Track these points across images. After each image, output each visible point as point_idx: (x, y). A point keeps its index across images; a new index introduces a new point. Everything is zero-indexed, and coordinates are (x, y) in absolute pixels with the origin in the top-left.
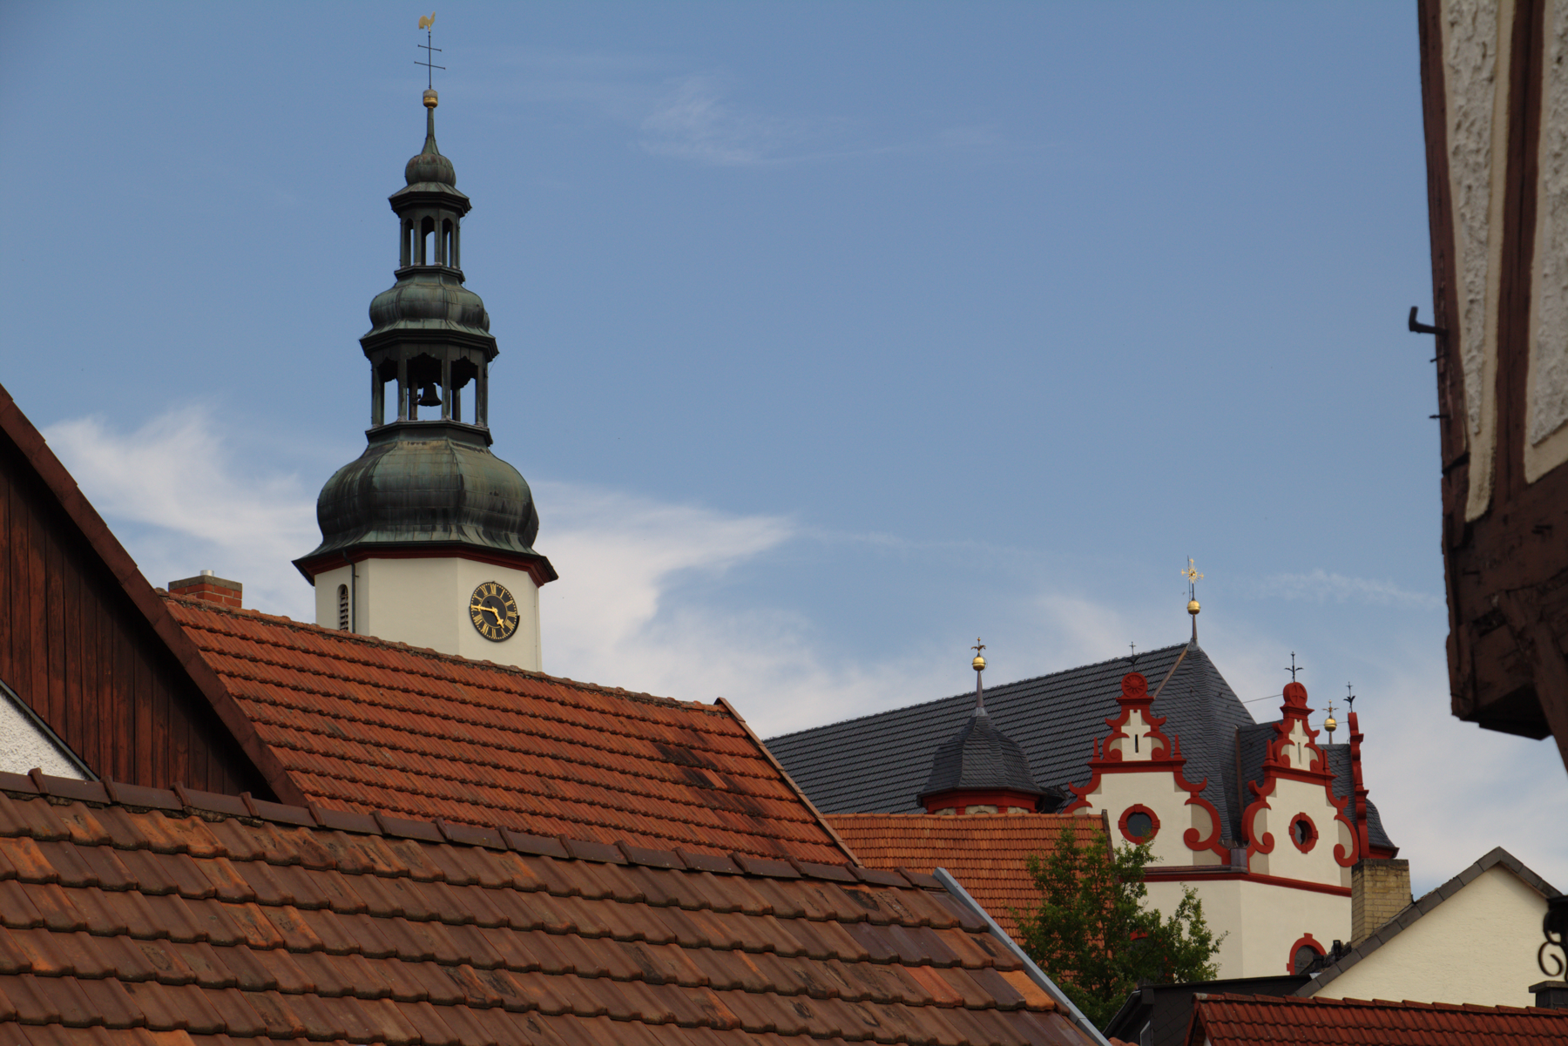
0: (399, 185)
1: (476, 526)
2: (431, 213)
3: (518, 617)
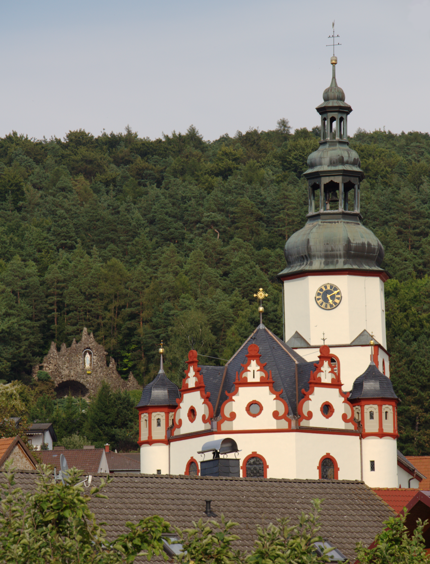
0: (320, 102)
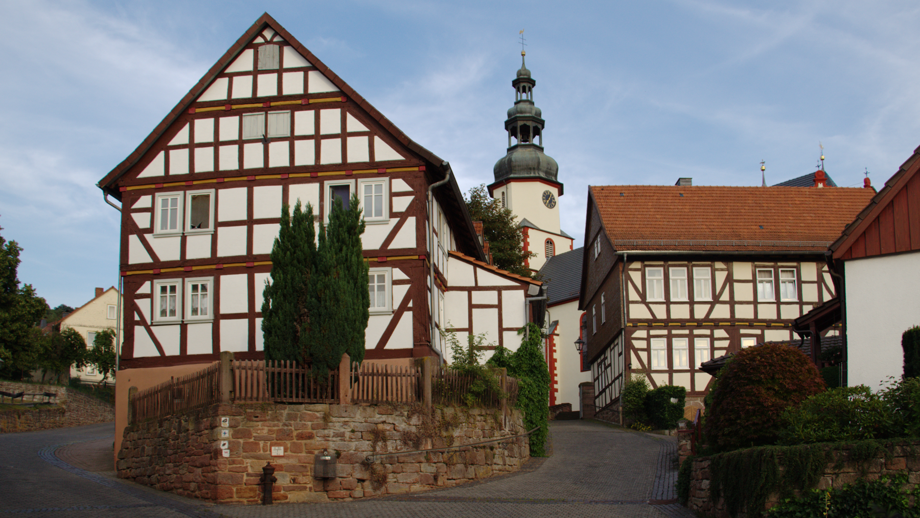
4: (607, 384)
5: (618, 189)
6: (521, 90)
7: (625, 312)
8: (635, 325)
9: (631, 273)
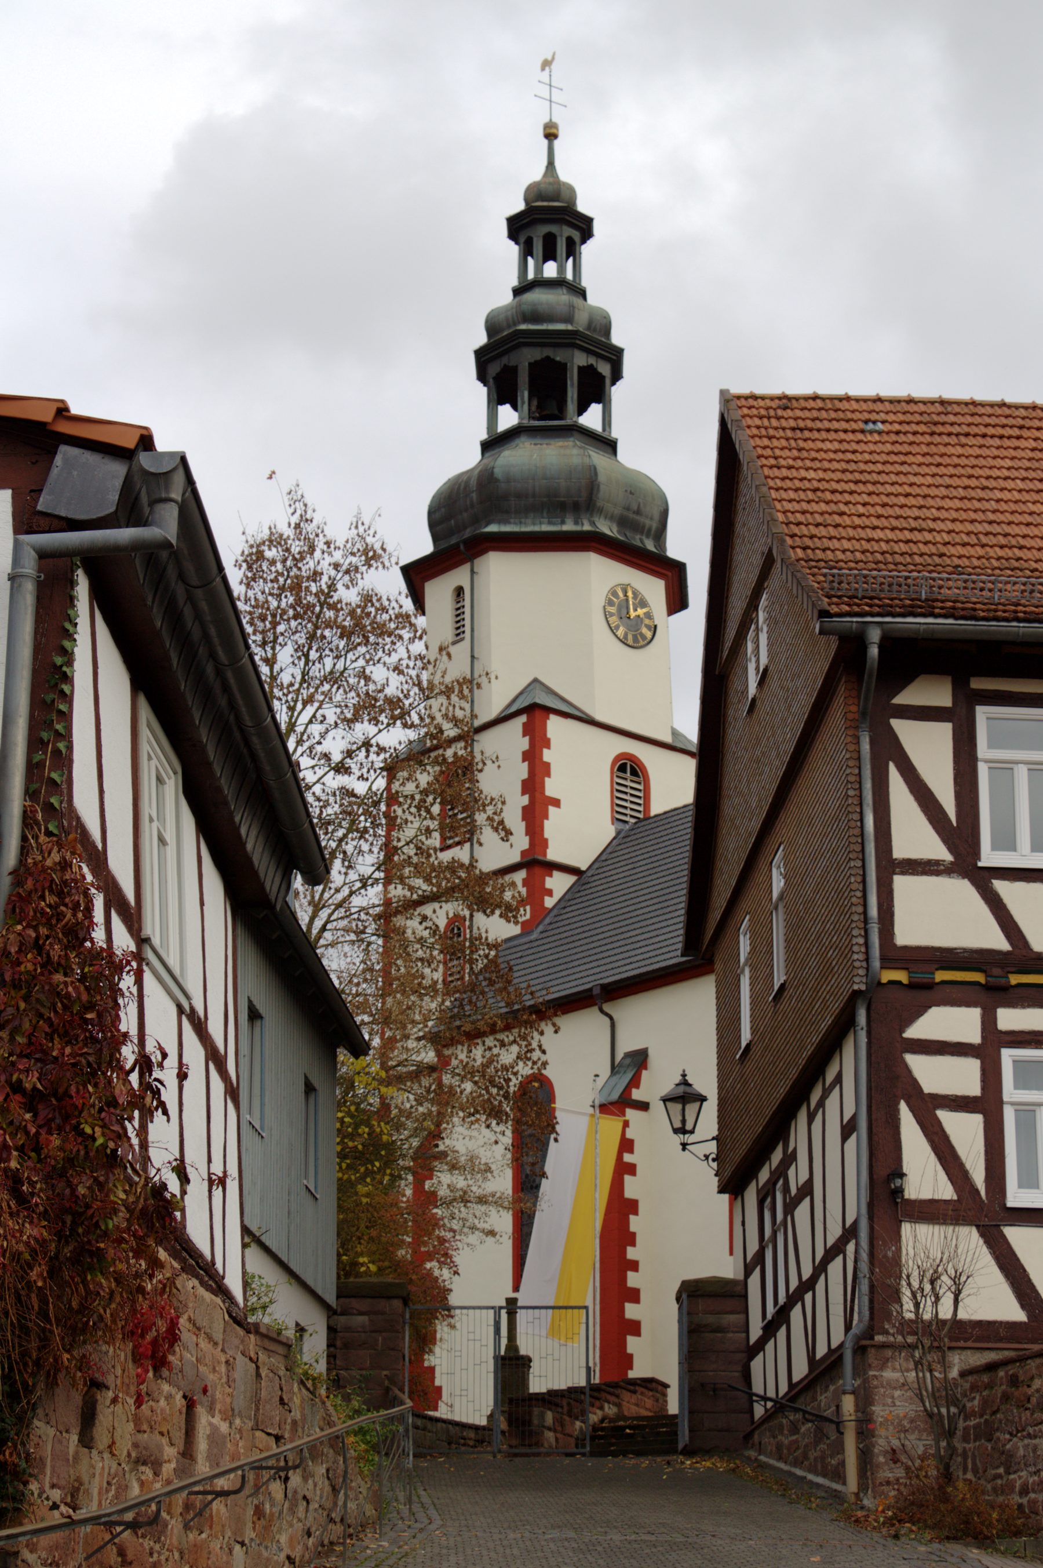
1: (609, 523)
2: (553, 228)
3: (656, 627)
4: (794, 1284)
5: (854, 405)
6: (538, 247)
7: (873, 911)
8: (921, 977)
9: (904, 729)
